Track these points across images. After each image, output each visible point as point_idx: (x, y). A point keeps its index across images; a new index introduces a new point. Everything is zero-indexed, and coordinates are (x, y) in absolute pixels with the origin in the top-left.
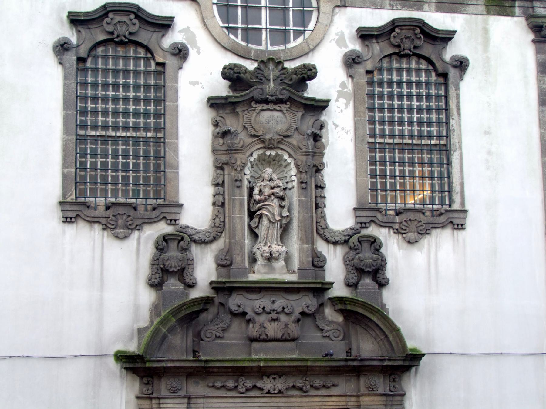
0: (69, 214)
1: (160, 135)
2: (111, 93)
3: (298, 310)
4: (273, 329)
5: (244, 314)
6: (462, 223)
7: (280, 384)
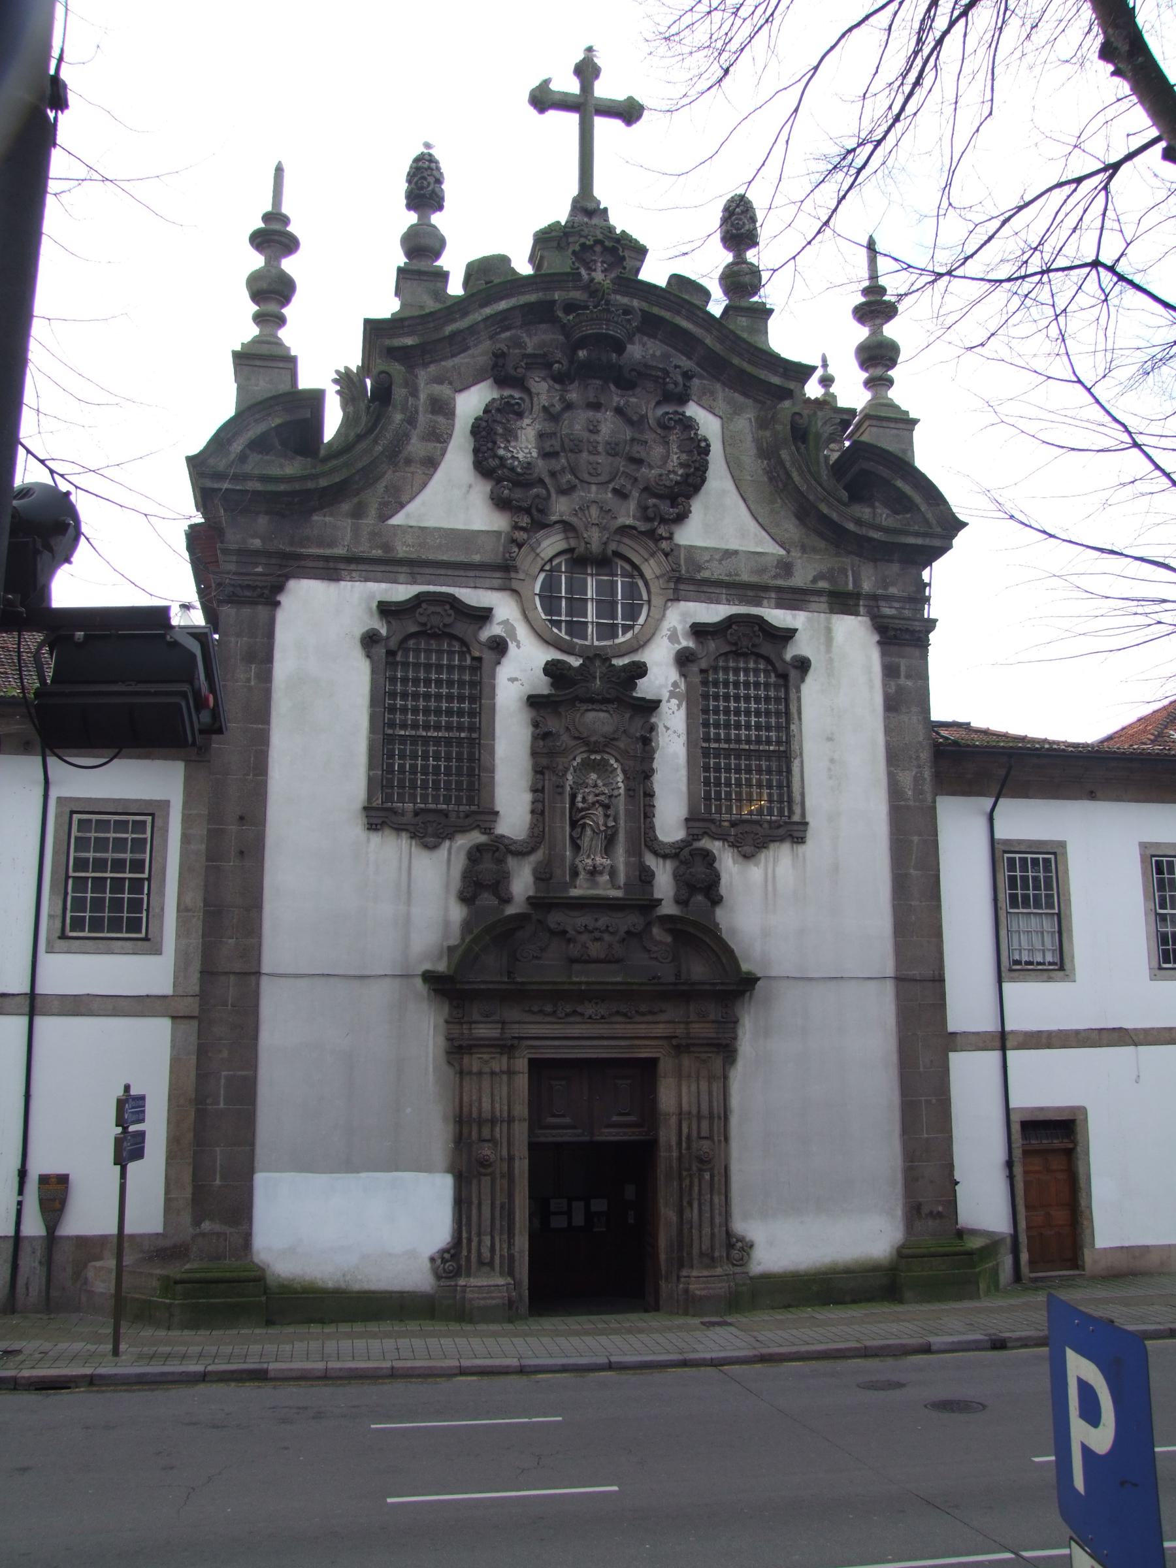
1: (475, 735)
4: (596, 950)
5: (565, 932)
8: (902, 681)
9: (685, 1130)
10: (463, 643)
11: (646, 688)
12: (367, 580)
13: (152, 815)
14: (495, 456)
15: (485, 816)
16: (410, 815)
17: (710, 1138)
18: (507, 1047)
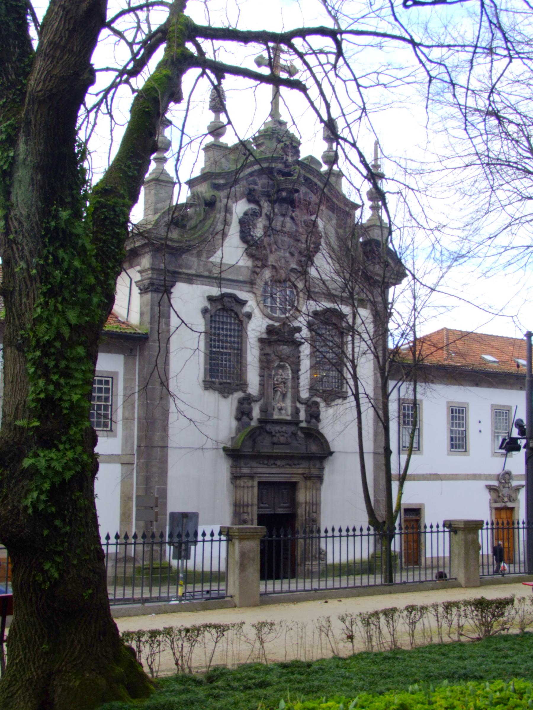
2: (217, 332)
3: (291, 432)
4: (282, 440)
5: (271, 433)
7: (283, 462)
9: (308, 509)
10: (236, 314)
12: (203, 284)
13: (112, 378)
14: (250, 235)
15: (243, 385)
16: (217, 383)
17: (316, 512)
18: (251, 477)
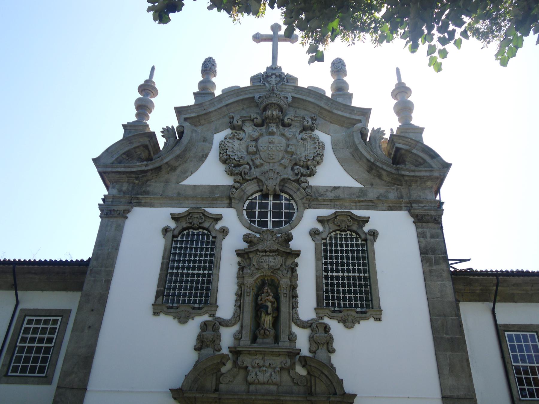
0: (157, 311)
6: (379, 317)
8: (428, 239)
11: (294, 245)
